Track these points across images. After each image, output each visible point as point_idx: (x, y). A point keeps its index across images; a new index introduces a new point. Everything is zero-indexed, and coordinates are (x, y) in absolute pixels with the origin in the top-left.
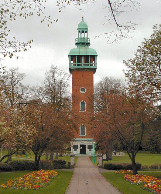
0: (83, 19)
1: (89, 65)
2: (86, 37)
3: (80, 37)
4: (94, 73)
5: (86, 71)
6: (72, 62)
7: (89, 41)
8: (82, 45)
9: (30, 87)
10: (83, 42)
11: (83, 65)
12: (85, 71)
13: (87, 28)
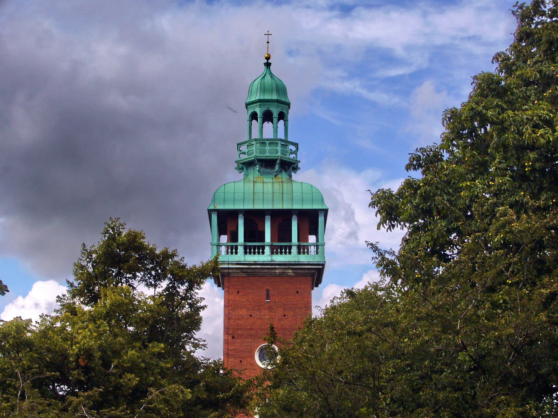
0: (268, 65)
1: (294, 250)
2: (281, 136)
3: (256, 135)
4: (317, 286)
5: (281, 275)
6: (224, 239)
7: (295, 153)
8: (262, 169)
9: (67, 289)
10: (268, 153)
11: (267, 250)
12: (275, 276)
13: (283, 99)
